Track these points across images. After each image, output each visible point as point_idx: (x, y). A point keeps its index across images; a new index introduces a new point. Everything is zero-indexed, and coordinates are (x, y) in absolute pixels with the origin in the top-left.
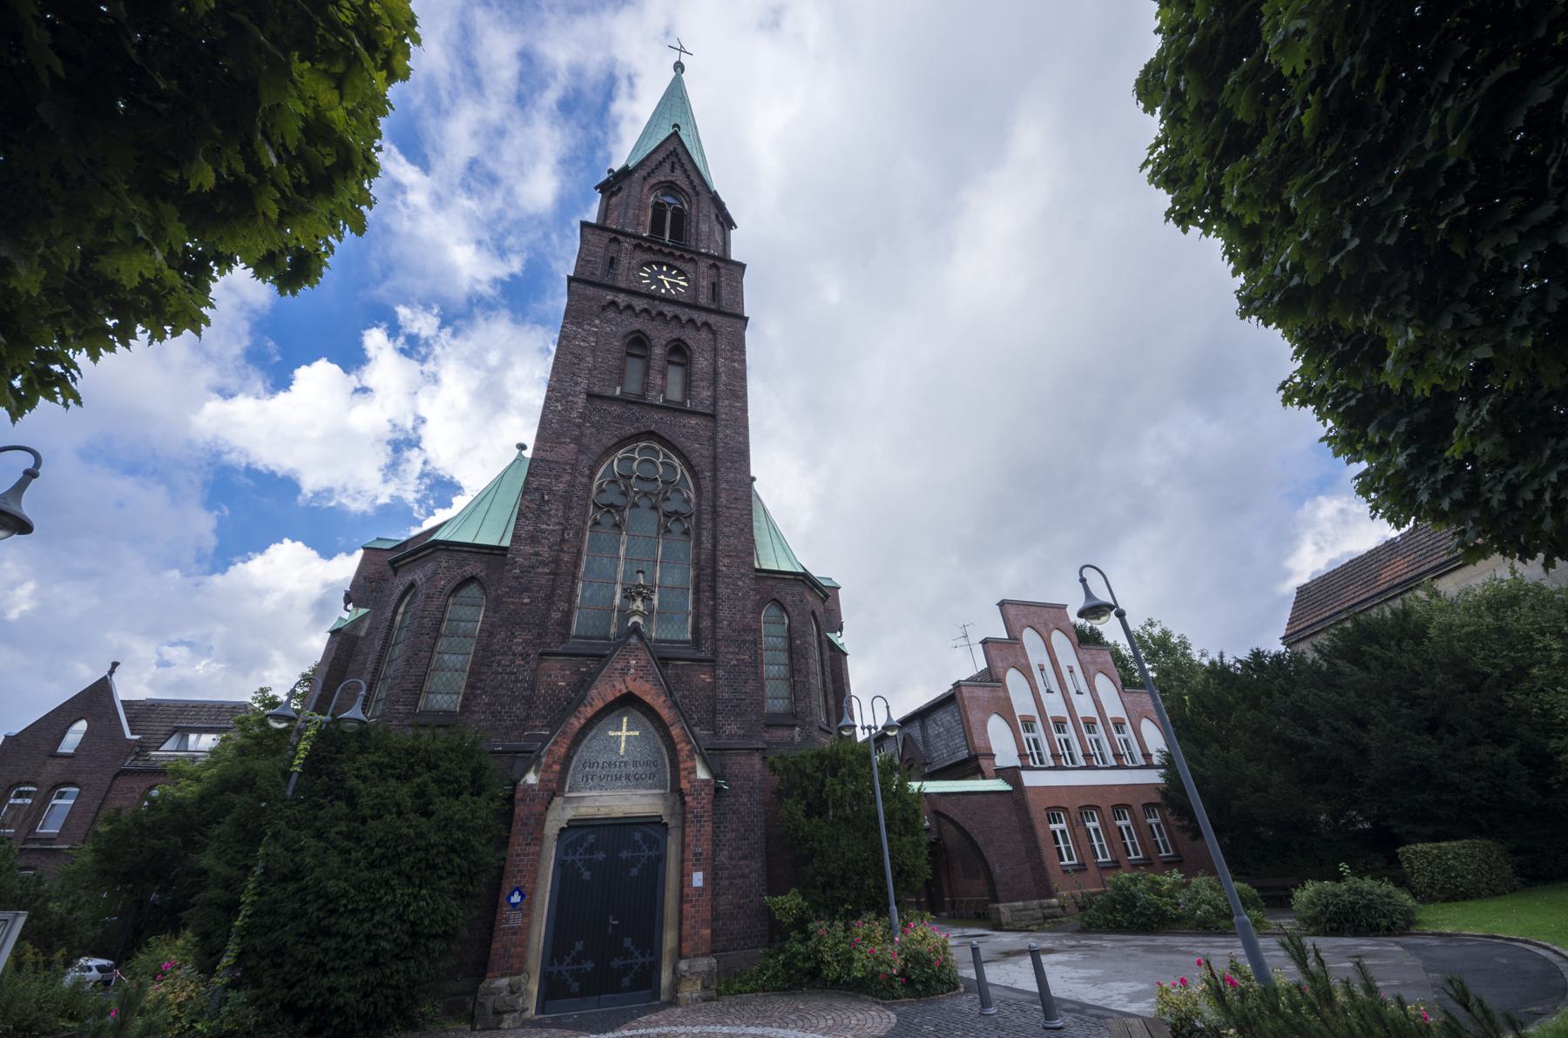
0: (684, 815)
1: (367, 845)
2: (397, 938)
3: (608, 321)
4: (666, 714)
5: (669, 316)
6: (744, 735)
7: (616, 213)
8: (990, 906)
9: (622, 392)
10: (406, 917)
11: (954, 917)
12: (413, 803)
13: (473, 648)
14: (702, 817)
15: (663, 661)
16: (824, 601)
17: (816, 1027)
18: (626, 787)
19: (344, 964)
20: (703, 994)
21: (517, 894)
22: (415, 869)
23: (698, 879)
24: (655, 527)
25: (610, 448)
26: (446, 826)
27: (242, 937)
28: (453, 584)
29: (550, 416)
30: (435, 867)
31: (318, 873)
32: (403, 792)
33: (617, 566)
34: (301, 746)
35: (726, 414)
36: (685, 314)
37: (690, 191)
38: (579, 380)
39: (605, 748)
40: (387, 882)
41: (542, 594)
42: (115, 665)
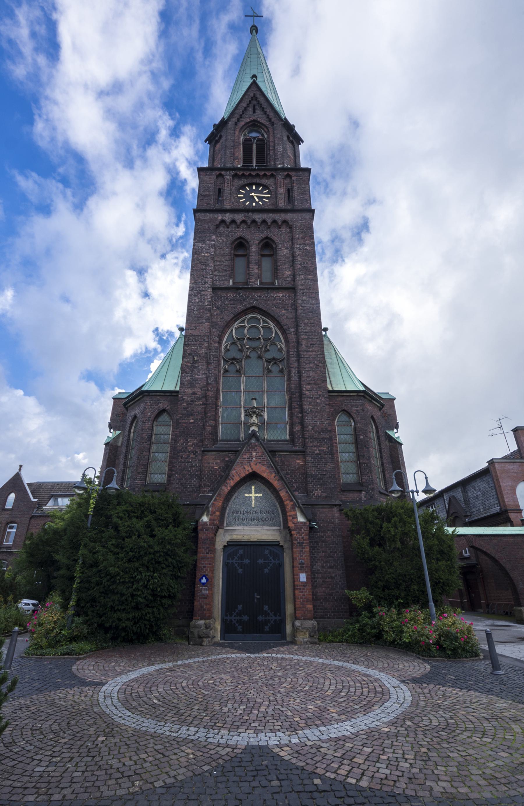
0: (292, 541)
1: (126, 551)
2: (146, 596)
3: (221, 235)
4: (276, 484)
5: (259, 221)
6: (327, 497)
7: (220, 156)
8: (514, 608)
9: (234, 283)
10: (148, 587)
11: (488, 613)
12: (145, 530)
13: (169, 449)
14: (303, 543)
15: (273, 453)
16: (380, 409)
17: (376, 666)
18: (257, 525)
19: (123, 607)
20: (310, 640)
21: (204, 578)
22: (150, 563)
23: (303, 577)
24: (261, 370)
25: (229, 321)
26: (162, 542)
27: (78, 593)
28: (154, 414)
29: (192, 307)
30: (159, 563)
31: (105, 563)
32: (139, 525)
33: (240, 397)
34: (91, 502)
35: (302, 285)
36: (269, 218)
37: (267, 124)
38: (207, 279)
39: (244, 503)
40: (137, 569)
41: (199, 417)
42: (21, 466)
